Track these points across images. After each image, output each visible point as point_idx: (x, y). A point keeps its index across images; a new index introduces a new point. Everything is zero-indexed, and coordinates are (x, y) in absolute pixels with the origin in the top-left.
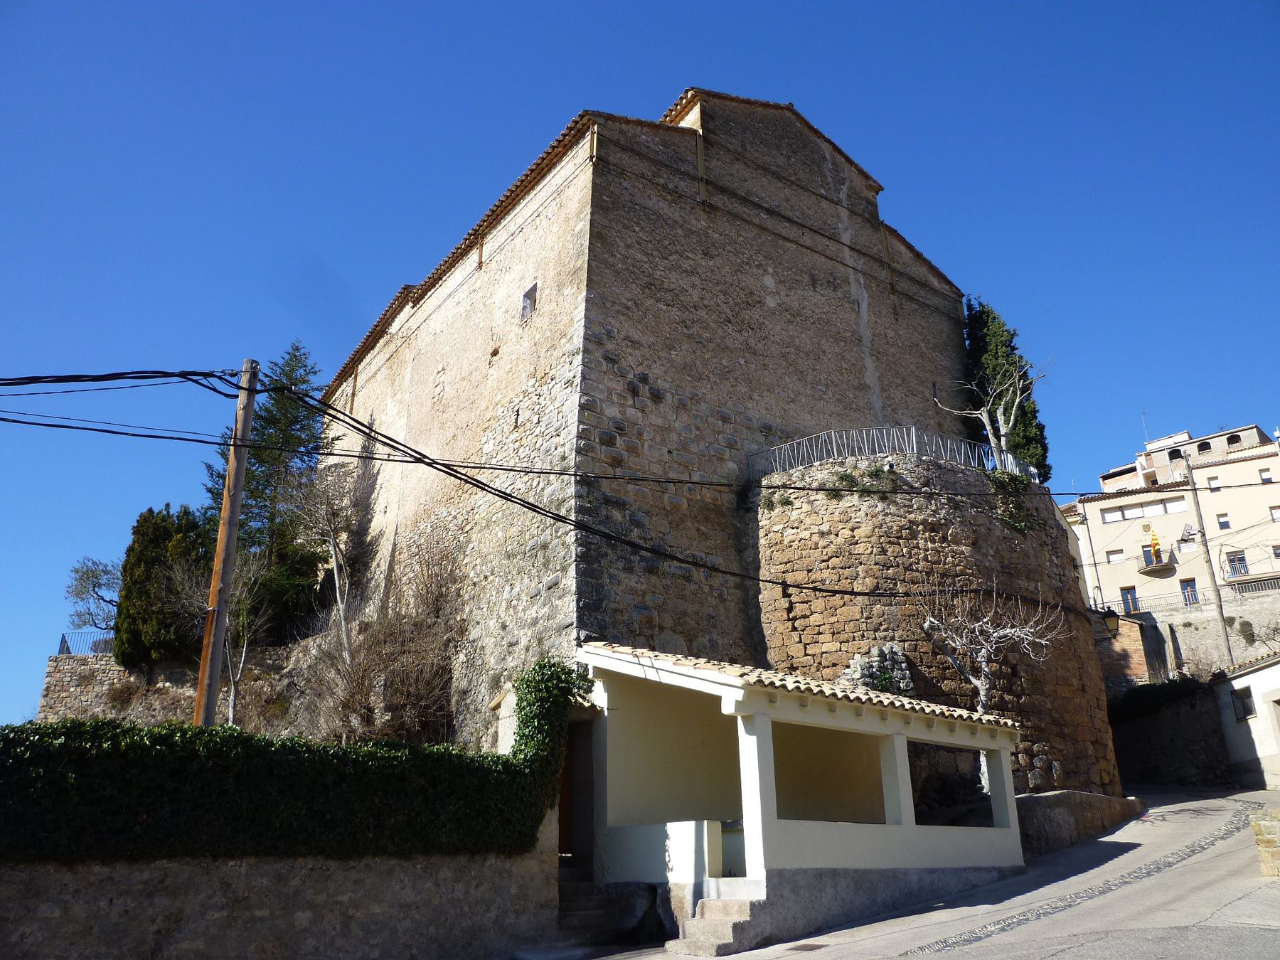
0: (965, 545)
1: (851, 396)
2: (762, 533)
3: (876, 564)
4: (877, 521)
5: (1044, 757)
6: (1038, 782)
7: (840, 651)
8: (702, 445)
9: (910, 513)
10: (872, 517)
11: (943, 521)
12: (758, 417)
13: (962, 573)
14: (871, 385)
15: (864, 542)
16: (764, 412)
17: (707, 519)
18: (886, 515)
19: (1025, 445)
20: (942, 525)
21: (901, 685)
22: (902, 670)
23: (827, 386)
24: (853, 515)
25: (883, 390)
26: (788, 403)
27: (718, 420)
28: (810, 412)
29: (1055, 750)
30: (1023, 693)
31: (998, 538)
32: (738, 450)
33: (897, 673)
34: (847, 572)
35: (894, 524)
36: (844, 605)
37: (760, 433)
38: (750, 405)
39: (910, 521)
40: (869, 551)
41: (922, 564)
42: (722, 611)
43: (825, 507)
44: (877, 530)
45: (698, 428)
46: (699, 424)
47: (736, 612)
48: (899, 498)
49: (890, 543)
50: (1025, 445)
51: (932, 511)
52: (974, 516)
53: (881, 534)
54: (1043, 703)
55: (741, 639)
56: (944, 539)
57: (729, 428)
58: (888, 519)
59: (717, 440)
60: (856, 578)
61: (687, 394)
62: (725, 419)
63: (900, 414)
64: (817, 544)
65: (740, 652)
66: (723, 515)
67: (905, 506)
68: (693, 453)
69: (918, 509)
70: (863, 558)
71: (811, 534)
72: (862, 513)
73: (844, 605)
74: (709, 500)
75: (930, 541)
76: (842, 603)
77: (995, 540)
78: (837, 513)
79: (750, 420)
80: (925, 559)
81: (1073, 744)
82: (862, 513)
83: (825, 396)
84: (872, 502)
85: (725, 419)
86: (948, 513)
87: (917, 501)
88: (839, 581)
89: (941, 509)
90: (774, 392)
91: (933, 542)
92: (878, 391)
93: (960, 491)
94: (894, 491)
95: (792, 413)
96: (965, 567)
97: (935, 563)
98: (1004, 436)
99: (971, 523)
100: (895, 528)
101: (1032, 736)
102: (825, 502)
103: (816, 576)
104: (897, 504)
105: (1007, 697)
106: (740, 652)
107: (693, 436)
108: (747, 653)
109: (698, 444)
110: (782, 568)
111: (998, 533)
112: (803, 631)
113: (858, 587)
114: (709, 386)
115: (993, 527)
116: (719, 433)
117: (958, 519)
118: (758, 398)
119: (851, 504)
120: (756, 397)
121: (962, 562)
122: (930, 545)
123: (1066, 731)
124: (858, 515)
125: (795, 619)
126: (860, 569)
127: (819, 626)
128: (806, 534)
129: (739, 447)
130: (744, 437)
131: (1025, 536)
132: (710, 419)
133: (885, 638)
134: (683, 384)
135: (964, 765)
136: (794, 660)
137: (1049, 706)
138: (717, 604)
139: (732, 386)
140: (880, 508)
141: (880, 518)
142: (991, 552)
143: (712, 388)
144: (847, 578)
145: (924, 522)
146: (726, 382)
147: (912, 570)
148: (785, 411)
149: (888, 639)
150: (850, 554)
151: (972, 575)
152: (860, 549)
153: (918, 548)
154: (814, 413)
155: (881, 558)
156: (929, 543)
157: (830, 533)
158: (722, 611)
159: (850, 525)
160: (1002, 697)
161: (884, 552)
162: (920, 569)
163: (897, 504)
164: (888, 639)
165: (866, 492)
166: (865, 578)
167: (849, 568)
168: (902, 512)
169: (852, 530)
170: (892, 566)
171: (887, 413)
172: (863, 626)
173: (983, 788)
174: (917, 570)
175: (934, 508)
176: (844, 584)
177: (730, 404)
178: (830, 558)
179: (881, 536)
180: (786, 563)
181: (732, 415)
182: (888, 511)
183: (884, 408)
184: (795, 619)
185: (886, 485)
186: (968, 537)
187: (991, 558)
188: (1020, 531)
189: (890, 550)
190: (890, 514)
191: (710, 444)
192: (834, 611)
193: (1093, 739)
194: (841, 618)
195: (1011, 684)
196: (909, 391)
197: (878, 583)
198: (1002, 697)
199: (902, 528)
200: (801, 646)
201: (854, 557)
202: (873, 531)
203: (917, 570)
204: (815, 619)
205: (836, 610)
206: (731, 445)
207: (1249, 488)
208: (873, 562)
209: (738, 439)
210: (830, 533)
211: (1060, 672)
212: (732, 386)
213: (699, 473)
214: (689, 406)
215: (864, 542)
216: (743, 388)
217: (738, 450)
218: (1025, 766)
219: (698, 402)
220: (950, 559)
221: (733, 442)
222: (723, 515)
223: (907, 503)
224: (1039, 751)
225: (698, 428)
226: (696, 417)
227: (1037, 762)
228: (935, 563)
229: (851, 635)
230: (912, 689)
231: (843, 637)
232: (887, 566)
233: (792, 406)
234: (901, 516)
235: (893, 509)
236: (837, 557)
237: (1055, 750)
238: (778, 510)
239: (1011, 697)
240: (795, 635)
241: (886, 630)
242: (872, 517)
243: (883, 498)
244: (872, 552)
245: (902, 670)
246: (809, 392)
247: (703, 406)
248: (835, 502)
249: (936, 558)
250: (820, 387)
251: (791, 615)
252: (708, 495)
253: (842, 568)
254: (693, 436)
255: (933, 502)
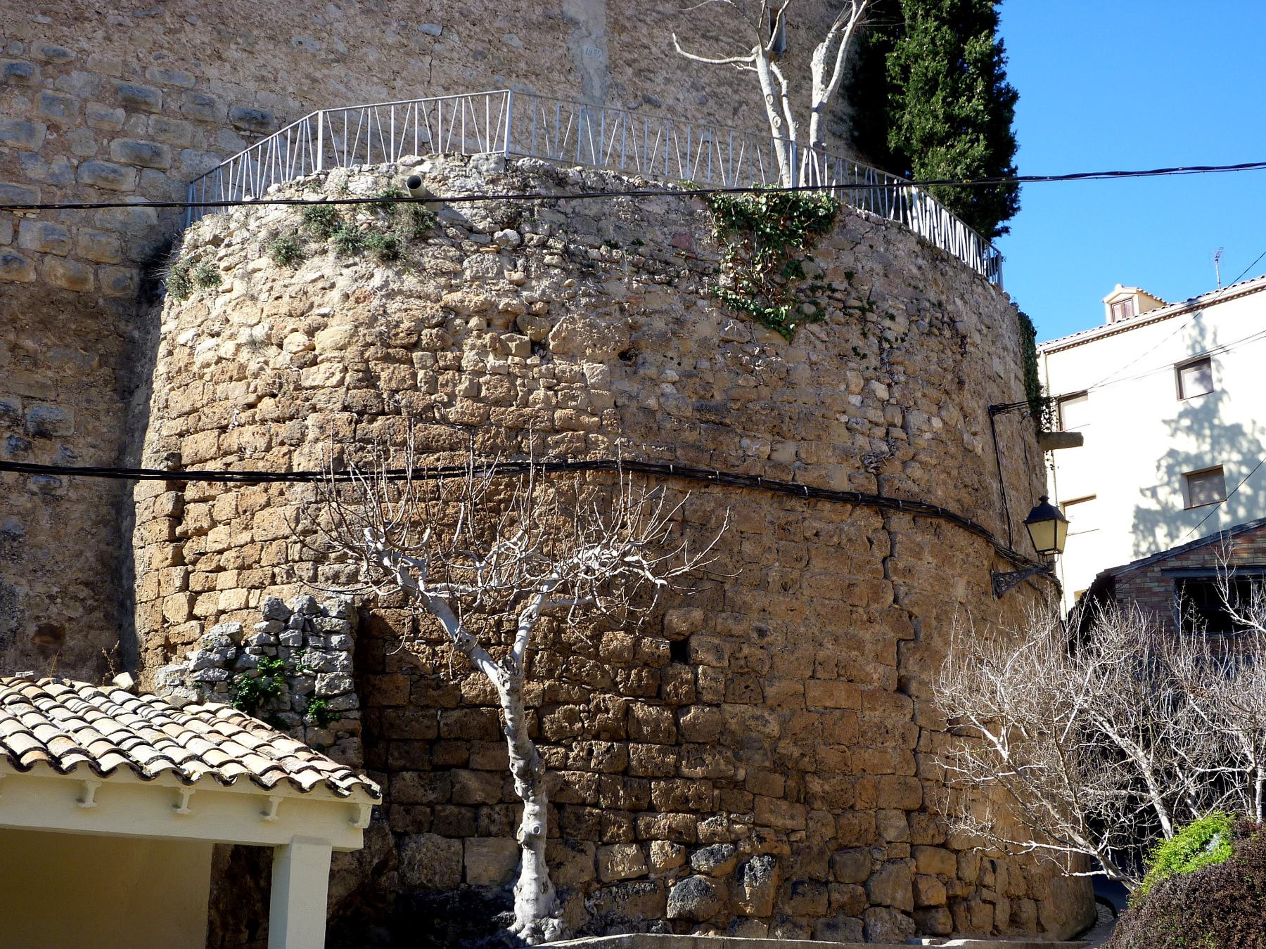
0: (592, 359)
1: (516, 42)
2: (163, 349)
3: (345, 408)
4: (362, 312)
5: (726, 848)
6: (691, 905)
7: (248, 608)
8: (60, 163)
9: (452, 289)
10: (357, 301)
11: (539, 305)
12: (232, 96)
13: (568, 425)
14: (582, 18)
15: (329, 360)
16: (251, 85)
17: (45, 324)
18: (391, 295)
19: (948, 136)
20: (536, 314)
21: (318, 685)
22: (327, 649)
23: (447, 25)
24: (317, 300)
25: (617, 26)
26: (326, 63)
27: (113, 106)
28: (386, 83)
29: (765, 832)
30: (696, 697)
31: (704, 343)
32: (164, 171)
33: (312, 658)
34: (285, 430)
35: (404, 313)
36: (268, 504)
37: (234, 134)
38: (212, 72)
39: (447, 309)
40: (334, 381)
41: (460, 405)
42: (45, 522)
43: (269, 284)
44: (362, 330)
45: (53, 127)
46: (57, 119)
47: (88, 525)
48: (430, 257)
49: (387, 359)
50: (948, 136)
51: (511, 282)
52: (636, 292)
53: (369, 339)
54: (752, 723)
55: (86, 584)
56: (537, 346)
57: (142, 125)
58: (393, 306)
59: (105, 151)
60: (301, 441)
61: (35, 52)
62: (133, 104)
63: (660, 80)
64: (242, 368)
65: (77, 612)
66: (98, 314)
67: (443, 274)
68: (31, 181)
69: (474, 279)
70: (320, 398)
71: (239, 346)
72: (335, 295)
73: (268, 504)
74: (62, 283)
75: (495, 350)
76: (263, 500)
77: (693, 346)
78: (286, 298)
79: (210, 104)
80: (474, 394)
81: (836, 817)
82: (335, 295)
83: (437, 47)
84: (362, 268)
85: (133, 104)
86: (557, 287)
87: (475, 263)
88: (269, 448)
89: (539, 278)
90: (287, 41)
91: (503, 352)
92: (599, 29)
93: (611, 234)
94: (421, 238)
95: (333, 85)
96: (580, 411)
97: (497, 403)
98: (816, 110)
99: (622, 310)
100: (406, 325)
101: (700, 798)
102: (270, 273)
103: (232, 439)
104: (421, 269)
105: (640, 710)
106: (77, 612)
107: (36, 144)
108: (98, 615)
109: (48, 162)
110: (180, 424)
111: (705, 329)
112: (194, 563)
113: (301, 463)
114: (100, 34)
115: (692, 317)
116: (113, 135)
117: (583, 301)
118: (237, 55)
119: (318, 274)
120: (233, 53)
121: (574, 398)
122: (491, 361)
123: (816, 785)
124: (326, 299)
125: (185, 537)
126: (312, 419)
127: (220, 552)
128: (227, 349)
129: (167, 163)
130: (185, 142)
131: (790, 336)
132: (94, 107)
133: (335, 578)
134: (27, 32)
135: (345, 863)
136: (173, 631)
137: (773, 728)
138: (35, 507)
139: (171, 31)
140: (377, 281)
141: (376, 302)
142: (672, 374)
143: (108, 39)
144: (282, 444)
145: (484, 310)
146: (150, 23)
147: (433, 420)
148: (315, 80)
149: (343, 579)
150: (298, 388)
151: (600, 428)
152: (314, 376)
153: (460, 370)
154: (399, 83)
155: (359, 396)
156: (491, 357)
157: (267, 342)
158: (45, 522)
159: (304, 323)
160: (627, 711)
161: (369, 380)
162: (452, 418)
163: (421, 269)
164: (343, 579)
165: (352, 246)
166: (317, 440)
167: (291, 418)
168: (430, 288)
169: (311, 333)
170: (383, 413)
171: (620, 79)
172: (295, 551)
173: (512, 920)
174: (444, 420)
175: (517, 276)
176: (275, 461)
177: (155, 70)
178: (260, 398)
179: (368, 345)
180: (188, 413)
181: (157, 98)
182: (395, 286)
183: (612, 67)
184: (185, 537)
185: (403, 227)
186: (604, 340)
187: (668, 389)
188: (776, 324)
189: (384, 375)
190: (400, 292)
191: (84, 159)
192: (245, 515)
193: (912, 803)
194: (259, 535)
195: (660, 678)
196: (695, 29)
197: (342, 451)
198: (627, 711)
199: (422, 323)
200: (182, 598)
201: (305, 393)
202: (355, 333)
203: (444, 420)
204: (217, 538)
205: (253, 515)
206: (143, 161)
207: (1242, 172)
208: (339, 405)
209: (166, 148)
210: (267, 342)
211: (829, 650)
212: (171, 31)
213: (39, 224)
214: (37, 78)
215: (329, 360)
216: (199, 36)
217: (164, 171)
218: (666, 869)
219: (65, 70)
220: (540, 393)
221: (147, 154)
222: (98, 314)
223: (448, 265)
224: (714, 834)
225: (53, 127)
226: (51, 101)
227: (700, 860)
228: (497, 403)
229: (268, 571)
230: (345, 693)
231: (255, 576)
232: (364, 414)
233: (338, 70)
234: (427, 297)
235: (410, 281)
236: (274, 396)
237: (765, 832)
238: (196, 293)
239: (653, 711)
240: (178, 572)
241: (342, 559)
242: (357, 301)
243: (390, 255)
244: (341, 383)
245: (327, 649)
246: (391, 39)
247: (78, 78)
248: (287, 271)
249: (501, 391)
250: (426, 27)
251: (178, 530)
252: (61, 271)
253: (277, 421)
254: (36, 144)
255: (520, 262)
